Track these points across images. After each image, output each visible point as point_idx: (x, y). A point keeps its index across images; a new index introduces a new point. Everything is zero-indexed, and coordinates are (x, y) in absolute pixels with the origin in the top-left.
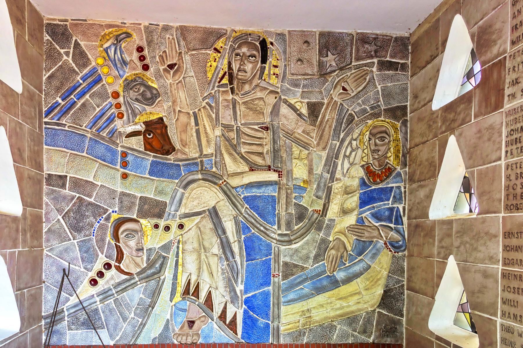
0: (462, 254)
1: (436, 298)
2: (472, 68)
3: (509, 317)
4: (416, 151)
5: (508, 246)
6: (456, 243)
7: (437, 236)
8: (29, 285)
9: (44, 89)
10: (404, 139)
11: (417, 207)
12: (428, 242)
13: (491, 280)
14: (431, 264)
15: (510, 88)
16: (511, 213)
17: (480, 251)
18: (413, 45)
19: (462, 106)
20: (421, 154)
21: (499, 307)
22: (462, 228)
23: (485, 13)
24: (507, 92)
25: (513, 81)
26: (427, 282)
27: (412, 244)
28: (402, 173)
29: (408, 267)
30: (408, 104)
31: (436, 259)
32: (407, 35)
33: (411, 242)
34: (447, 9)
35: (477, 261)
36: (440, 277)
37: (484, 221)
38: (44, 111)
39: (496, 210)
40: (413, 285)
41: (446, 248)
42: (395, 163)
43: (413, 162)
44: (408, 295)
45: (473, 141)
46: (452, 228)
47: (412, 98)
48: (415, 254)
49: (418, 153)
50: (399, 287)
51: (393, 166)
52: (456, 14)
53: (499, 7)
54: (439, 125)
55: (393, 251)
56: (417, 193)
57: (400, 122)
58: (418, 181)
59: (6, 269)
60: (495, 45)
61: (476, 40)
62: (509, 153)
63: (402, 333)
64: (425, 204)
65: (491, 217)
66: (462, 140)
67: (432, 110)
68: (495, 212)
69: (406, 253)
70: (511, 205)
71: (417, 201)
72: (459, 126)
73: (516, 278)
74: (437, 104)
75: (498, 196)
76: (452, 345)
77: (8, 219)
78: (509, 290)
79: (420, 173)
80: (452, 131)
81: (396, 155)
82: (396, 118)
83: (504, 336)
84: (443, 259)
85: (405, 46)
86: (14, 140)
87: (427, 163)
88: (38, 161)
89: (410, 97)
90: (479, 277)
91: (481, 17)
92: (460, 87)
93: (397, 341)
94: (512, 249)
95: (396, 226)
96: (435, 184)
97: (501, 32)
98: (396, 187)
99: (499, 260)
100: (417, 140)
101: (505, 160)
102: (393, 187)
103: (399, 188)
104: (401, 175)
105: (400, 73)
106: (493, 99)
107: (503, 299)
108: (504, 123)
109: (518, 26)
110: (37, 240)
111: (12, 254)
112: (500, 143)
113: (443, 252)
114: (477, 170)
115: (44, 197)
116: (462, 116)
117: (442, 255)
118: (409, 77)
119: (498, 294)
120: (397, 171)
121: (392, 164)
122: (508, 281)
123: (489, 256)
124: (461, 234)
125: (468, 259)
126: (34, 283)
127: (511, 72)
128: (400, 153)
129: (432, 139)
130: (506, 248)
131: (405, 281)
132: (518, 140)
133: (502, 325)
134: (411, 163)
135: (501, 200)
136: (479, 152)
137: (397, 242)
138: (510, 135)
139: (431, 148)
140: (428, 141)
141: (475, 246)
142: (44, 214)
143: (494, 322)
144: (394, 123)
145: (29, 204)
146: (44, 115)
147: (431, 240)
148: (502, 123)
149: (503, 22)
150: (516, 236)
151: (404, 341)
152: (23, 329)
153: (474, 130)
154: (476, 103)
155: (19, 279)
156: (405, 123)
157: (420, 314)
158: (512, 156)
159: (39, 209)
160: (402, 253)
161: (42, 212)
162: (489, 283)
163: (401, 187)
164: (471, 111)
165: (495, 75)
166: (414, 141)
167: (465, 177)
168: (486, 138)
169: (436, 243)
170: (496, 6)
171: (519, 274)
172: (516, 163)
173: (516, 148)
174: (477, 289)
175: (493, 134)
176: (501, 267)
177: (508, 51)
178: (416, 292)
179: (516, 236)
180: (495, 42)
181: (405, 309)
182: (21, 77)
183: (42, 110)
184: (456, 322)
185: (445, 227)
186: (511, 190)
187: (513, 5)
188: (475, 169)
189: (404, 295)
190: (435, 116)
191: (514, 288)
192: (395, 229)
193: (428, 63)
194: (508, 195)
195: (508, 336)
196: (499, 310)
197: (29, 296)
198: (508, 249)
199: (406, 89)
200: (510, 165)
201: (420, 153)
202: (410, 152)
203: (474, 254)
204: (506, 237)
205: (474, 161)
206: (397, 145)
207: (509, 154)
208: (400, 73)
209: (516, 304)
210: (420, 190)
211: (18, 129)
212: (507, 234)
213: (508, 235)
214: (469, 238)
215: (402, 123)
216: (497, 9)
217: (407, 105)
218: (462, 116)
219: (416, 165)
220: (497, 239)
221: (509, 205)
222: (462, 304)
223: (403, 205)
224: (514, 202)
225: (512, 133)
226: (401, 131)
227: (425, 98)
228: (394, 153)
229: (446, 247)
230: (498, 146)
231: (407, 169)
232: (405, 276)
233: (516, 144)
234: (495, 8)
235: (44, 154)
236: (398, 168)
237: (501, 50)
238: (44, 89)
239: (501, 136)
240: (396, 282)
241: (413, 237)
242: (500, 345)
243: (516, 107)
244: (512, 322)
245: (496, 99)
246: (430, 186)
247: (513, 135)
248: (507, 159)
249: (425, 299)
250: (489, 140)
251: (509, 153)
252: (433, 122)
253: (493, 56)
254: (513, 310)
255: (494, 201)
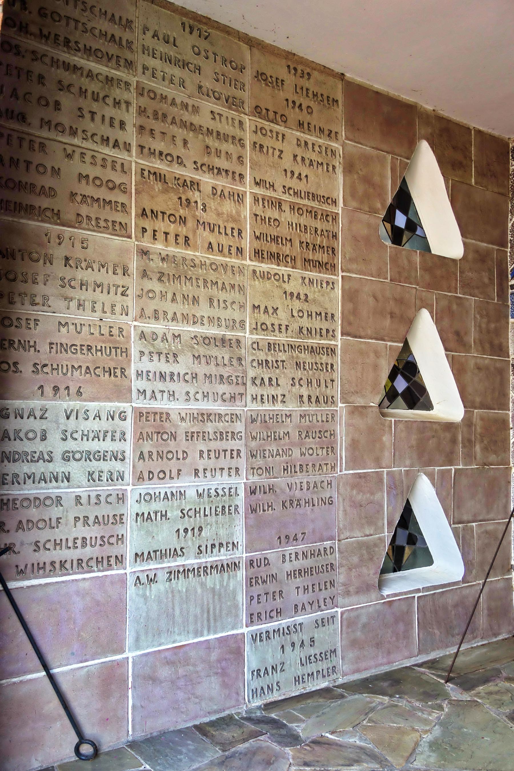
8: (481, 518)
9: (511, 240)
38: (510, 270)
59: (435, 492)
74: (425, 315)
77: (435, 426)
86: (446, 322)
88: (496, 342)
110: (495, 454)
111: (442, 473)
115: (511, 392)
126: (491, 516)
142: (511, 416)
145: (477, 405)
146: (510, 276)
152: (468, 578)
155: (458, 506)
159: (499, 410)
161: (508, 415)
182: (460, 237)
183: (508, 269)
197: (483, 533)
211: (455, 307)
235: (510, 330)
238: (511, 240)
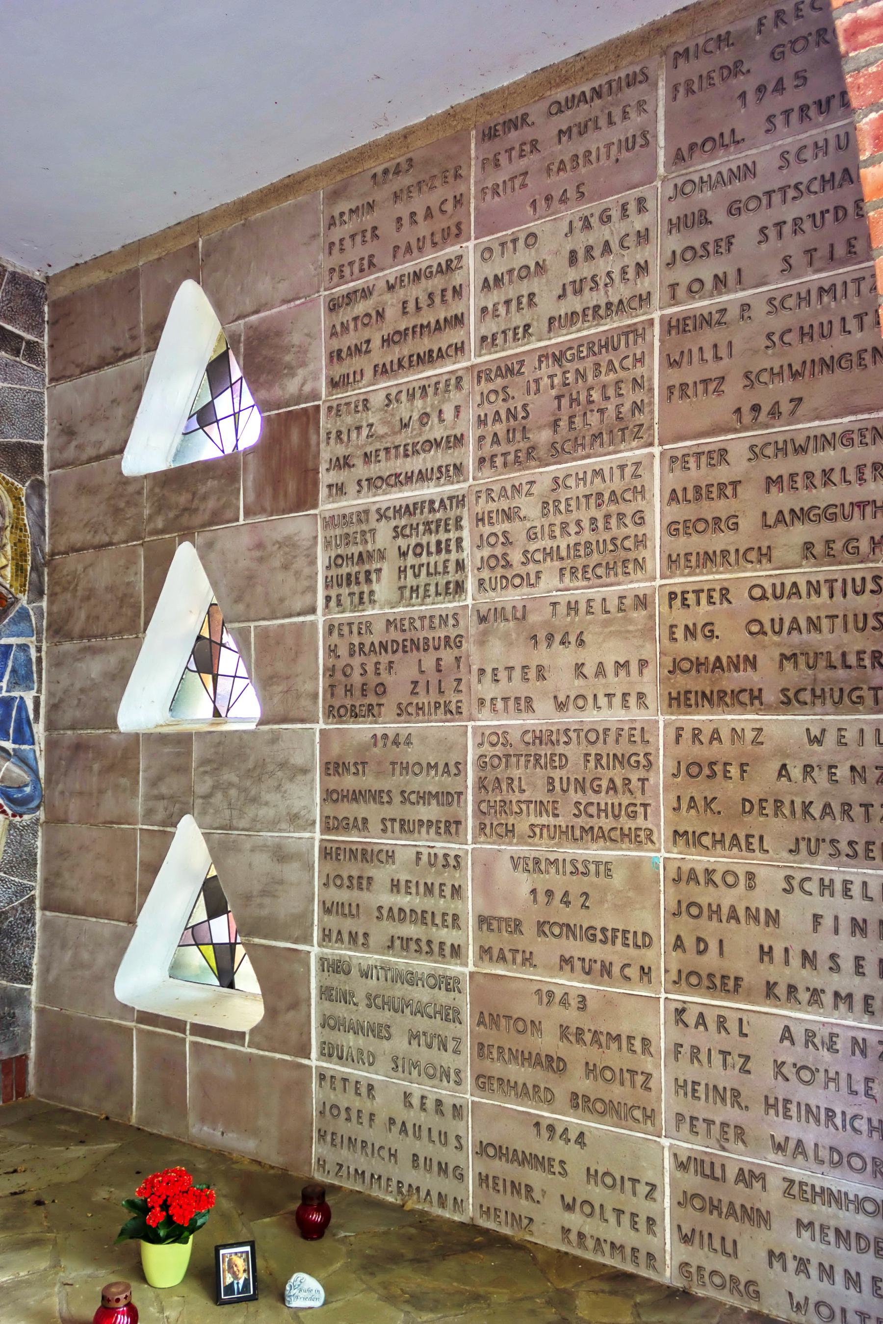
0: (216, 811)
1: (140, 921)
2: (210, 404)
3: (340, 939)
4: (72, 563)
5: (334, 791)
6: (202, 787)
7: (144, 771)
10: (37, 529)
11: (79, 700)
12: (116, 786)
13: (296, 865)
14: (128, 840)
15: (332, 472)
16: (341, 723)
17: (267, 804)
18: (54, 306)
19: (211, 483)
20: (90, 571)
21: (316, 922)
22: (216, 753)
23: (263, 301)
24: (326, 477)
25: (338, 459)
26: (111, 883)
27: (62, 793)
28: (31, 613)
29: (47, 852)
30: (45, 443)
31: (140, 826)
32: (38, 276)
33: (60, 787)
34: (159, 259)
35: (259, 826)
36: (153, 869)
37: (275, 738)
39: (305, 715)
40: (57, 893)
41: (172, 799)
42: (17, 585)
43: (65, 589)
44: (46, 925)
45: (243, 563)
46: (189, 753)
47: (56, 433)
48: (73, 816)
49: (80, 568)
50: (21, 904)
51: (11, 593)
52: (186, 278)
53: (298, 302)
54: (147, 512)
55: (10, 812)
56: (78, 665)
57: (27, 484)
58: (81, 637)
60: (293, 375)
61: (242, 350)
62: (334, 600)
63: (28, 1026)
64: (106, 693)
65: (294, 730)
66: (212, 556)
67: (121, 473)
68: (302, 721)
69: (41, 814)
70: (341, 707)
71: (78, 686)
72: (203, 526)
73: (356, 858)
75: (308, 687)
76: (188, 1027)
78: (338, 882)
79: (88, 618)
80: (187, 534)
81: (17, 565)
82: (16, 471)
83: (328, 983)
84: (164, 824)
85: (36, 302)
87: (109, 596)
89: (50, 429)
90: (262, 862)
91: (254, 309)
92: (180, 437)
93: (15, 1049)
94: (344, 796)
95: (17, 746)
96: (136, 648)
97: (306, 352)
98: (19, 646)
99: (314, 822)
100: (77, 537)
101: (324, 615)
102: (11, 646)
103: (24, 648)
104: (29, 616)
105: (24, 362)
106: (292, 487)
107: (324, 902)
108: (320, 539)
109: (344, 355)
112: (313, 577)
113: (161, 810)
114: (256, 627)
116: (211, 504)
117: (160, 815)
118: (47, 380)
119: (313, 894)
120: (20, 605)
121: (8, 586)
122: (336, 863)
123: (288, 814)
124: (215, 766)
125: (234, 822)
127: (332, 441)
128: (26, 561)
129: (126, 542)
130: (329, 796)
131: (38, 887)
132: (353, 578)
133: (322, 960)
134: (58, 589)
135: (316, 696)
136: (259, 589)
137: (19, 787)
138: (336, 565)
139: (122, 562)
140: (111, 544)
141: (253, 792)
143: (303, 955)
144: (13, 484)
147: (124, 781)
148: (316, 537)
149: (308, 335)
150: (353, 770)
151: (33, 1044)
153: (245, 540)
154: (250, 484)
156: (38, 487)
157: (83, 966)
158: (340, 608)
160: (30, 816)
162: (292, 872)
163: (28, 647)
164: (238, 499)
165: (295, 436)
166: (65, 537)
167: (199, 638)
168: (277, 563)
169: (141, 789)
170: (290, 297)
171: (360, 847)
172: (350, 624)
173: (350, 594)
174: (257, 887)
175: (295, 557)
176: (318, 836)
177: (323, 397)
178: (75, 913)
179: (353, 770)
180: (291, 371)
181: (35, 961)
184: (176, 970)
185: (167, 750)
186: (339, 675)
187: (331, 310)
188: (252, 625)
189: (34, 925)
190: (131, 489)
191: (350, 877)
192: (15, 755)
193: (103, 363)
194: (332, 686)
195: (336, 981)
196: (316, 928)
198: (335, 796)
199: (40, 407)
200: (336, 625)
201: (85, 569)
202: (54, 562)
203: (251, 811)
204: (331, 772)
205: (248, 606)
206: (20, 541)
207: (333, 603)
208: (24, 362)
209: (354, 912)
210: (88, 657)
212: (331, 767)
213: (333, 767)
214: (237, 776)
215: (32, 486)
216: (292, 304)
217: (41, 446)
218: (211, 504)
219: (74, 596)
220: (309, 777)
221: (337, 707)
222: (193, 927)
223: (33, 693)
224: (348, 702)
225: (340, 561)
226: (29, 506)
227: (101, 443)
228: (13, 559)
229: (172, 797)
230: (306, 583)
231: (44, 604)
232: (38, 874)
233: (349, 585)
234: (289, 301)
236: (24, 599)
237: (307, 388)
239: (313, 562)
240: (15, 894)
241: (66, 774)
242: (317, 1003)
243: (347, 511)
244: (346, 949)
245: (298, 490)
246: (122, 653)
247: (341, 566)
248: (330, 613)
249: (105, 927)
250: (286, 567)
251: (334, 600)
252: (128, 503)
253: (287, 396)
254: (348, 925)
255: (298, 697)
